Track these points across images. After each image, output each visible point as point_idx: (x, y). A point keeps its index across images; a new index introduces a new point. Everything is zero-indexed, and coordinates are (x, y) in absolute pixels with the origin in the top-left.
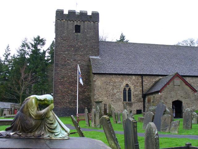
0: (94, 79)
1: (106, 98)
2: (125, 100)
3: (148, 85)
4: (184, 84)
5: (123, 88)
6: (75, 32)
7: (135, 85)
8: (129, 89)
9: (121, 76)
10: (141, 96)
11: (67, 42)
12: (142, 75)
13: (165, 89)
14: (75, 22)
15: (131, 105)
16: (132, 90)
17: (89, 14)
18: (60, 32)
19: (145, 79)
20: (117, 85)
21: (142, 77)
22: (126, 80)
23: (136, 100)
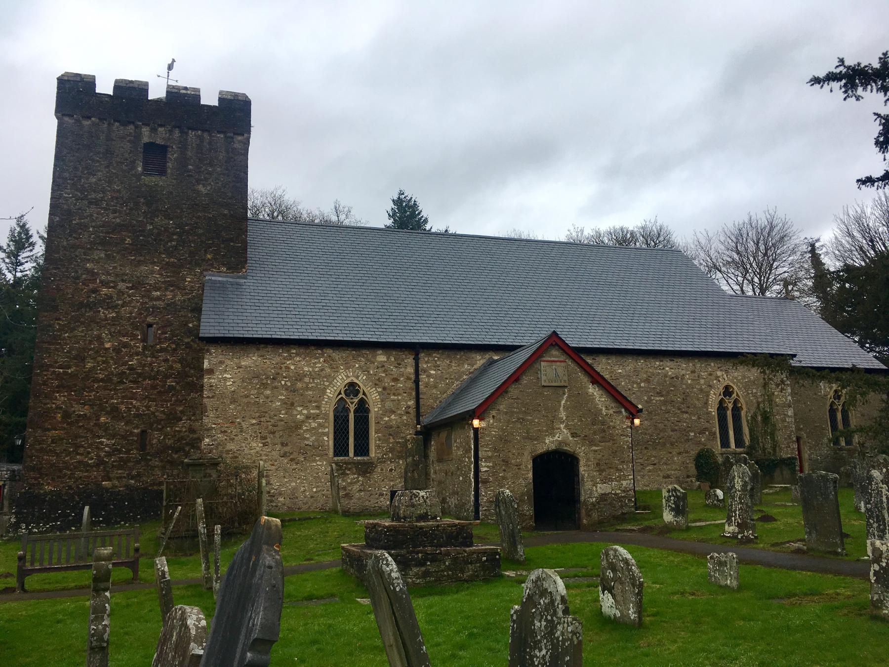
0: (206, 365)
1: (257, 445)
2: (340, 448)
3: (442, 385)
4: (584, 379)
5: (334, 401)
6: (144, 169)
7: (384, 389)
8: (736, 402)
9: (329, 351)
10: (409, 434)
11: (105, 209)
12: (415, 349)
13: (503, 405)
14: (160, 129)
15: (365, 469)
16: (374, 409)
17: (209, 99)
18: (76, 169)
19: (427, 362)
20: (307, 389)
21: (417, 355)
22: (347, 368)
23: (392, 450)
